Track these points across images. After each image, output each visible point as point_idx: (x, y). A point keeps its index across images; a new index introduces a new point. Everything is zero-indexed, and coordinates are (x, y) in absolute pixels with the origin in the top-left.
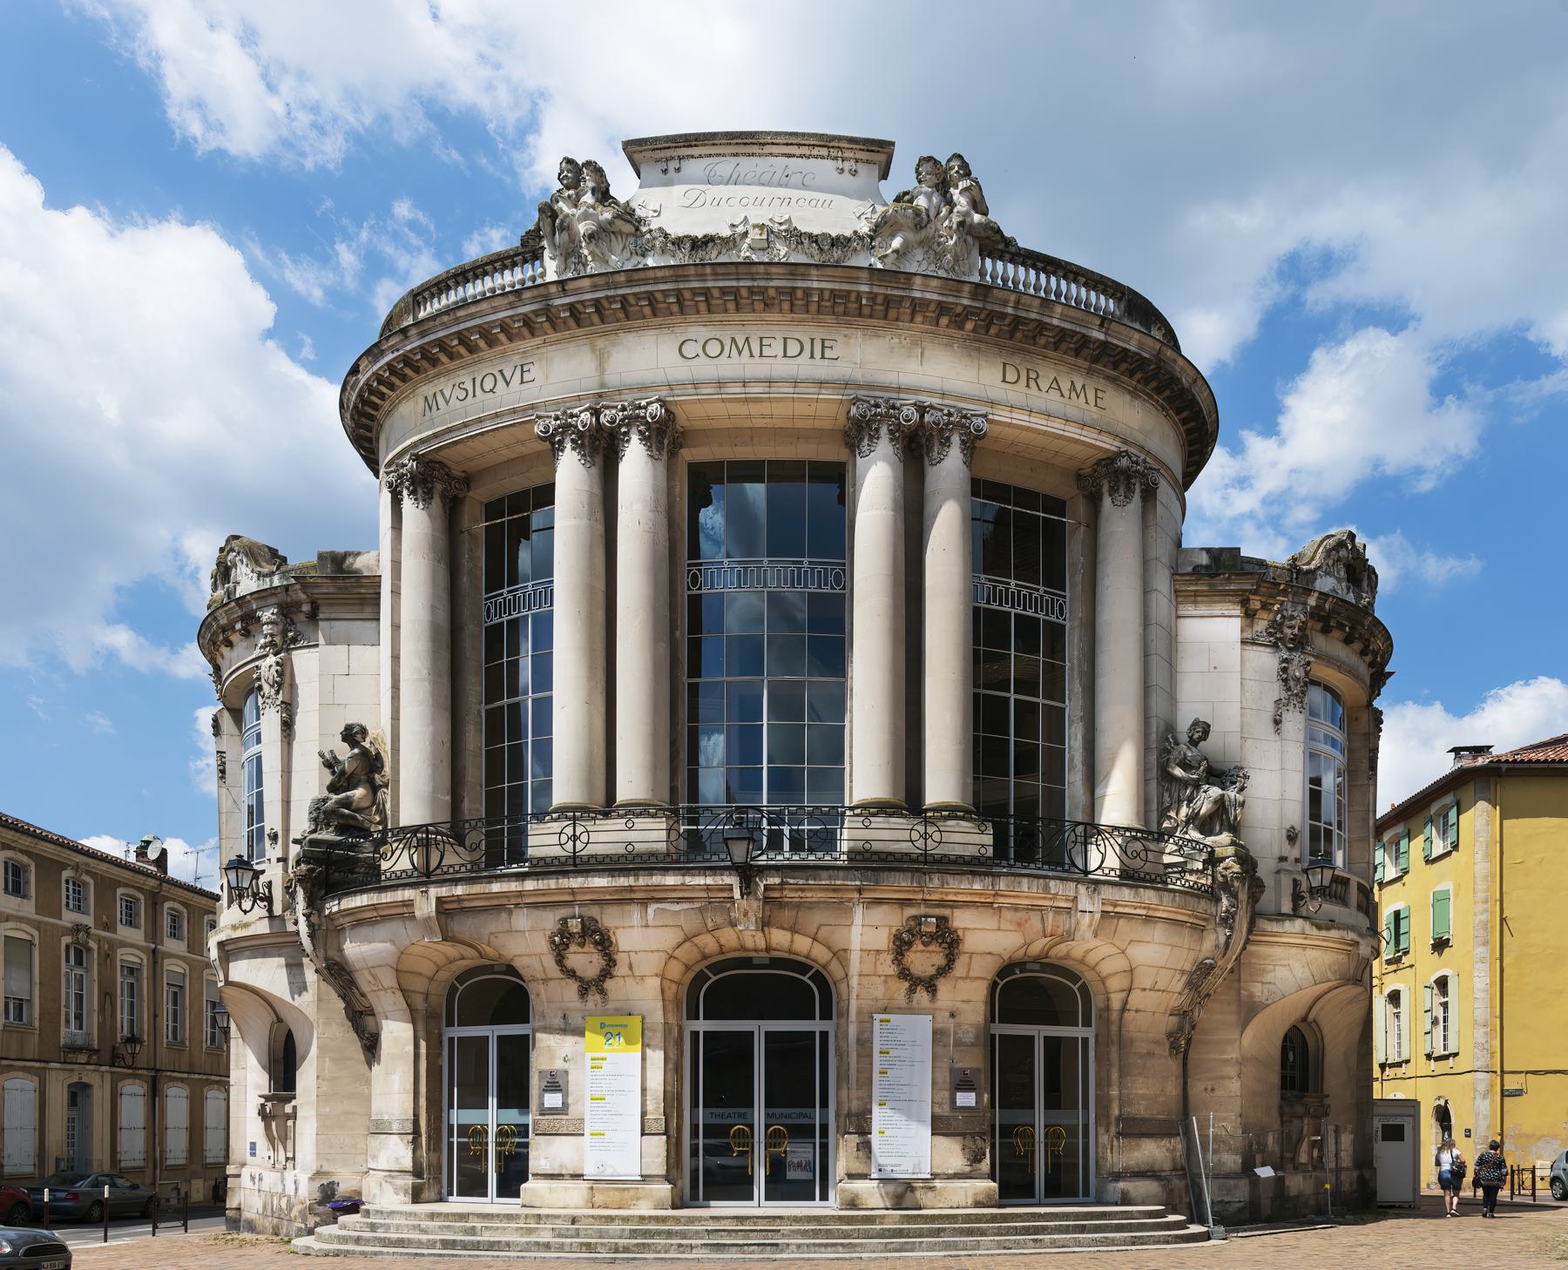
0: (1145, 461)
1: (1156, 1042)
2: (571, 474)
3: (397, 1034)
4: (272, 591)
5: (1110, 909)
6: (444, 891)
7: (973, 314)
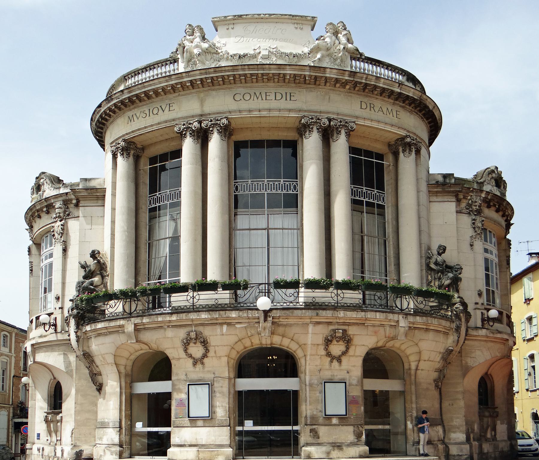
0: (416, 139)
1: (430, 384)
2: (189, 147)
3: (112, 385)
4: (61, 195)
5: (411, 325)
6: (138, 320)
7: (349, 83)
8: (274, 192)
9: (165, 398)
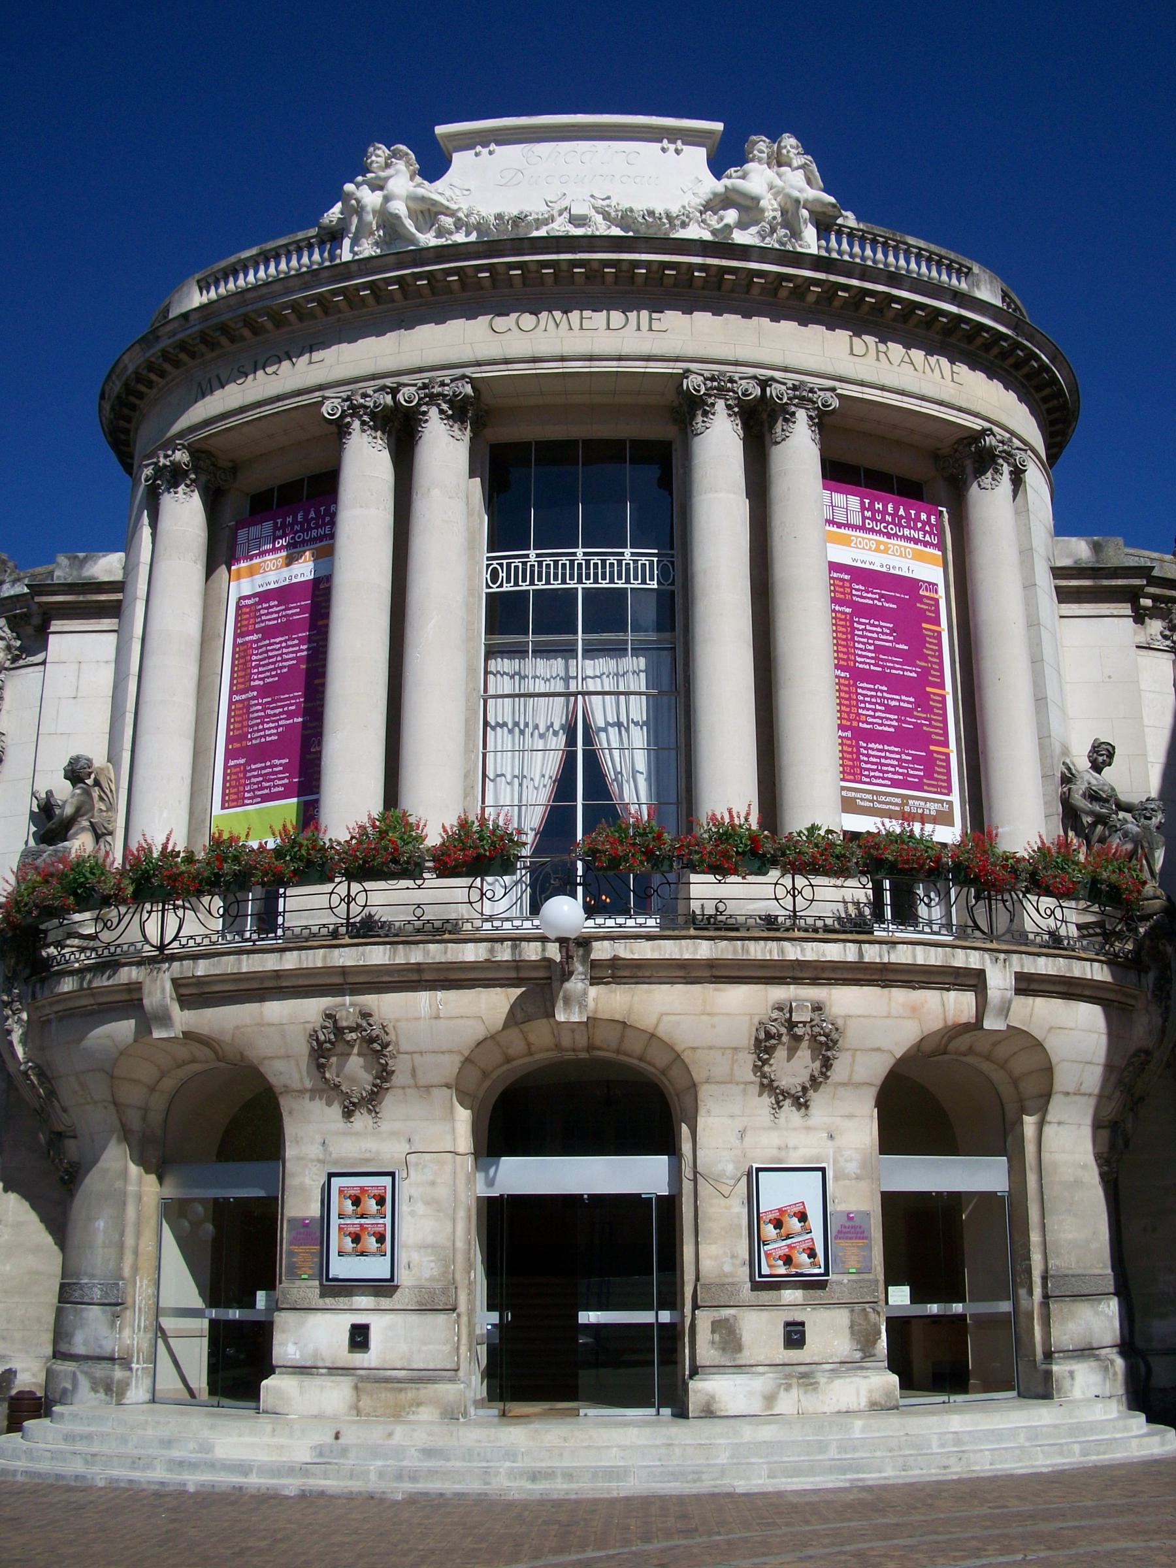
8: (604, 584)
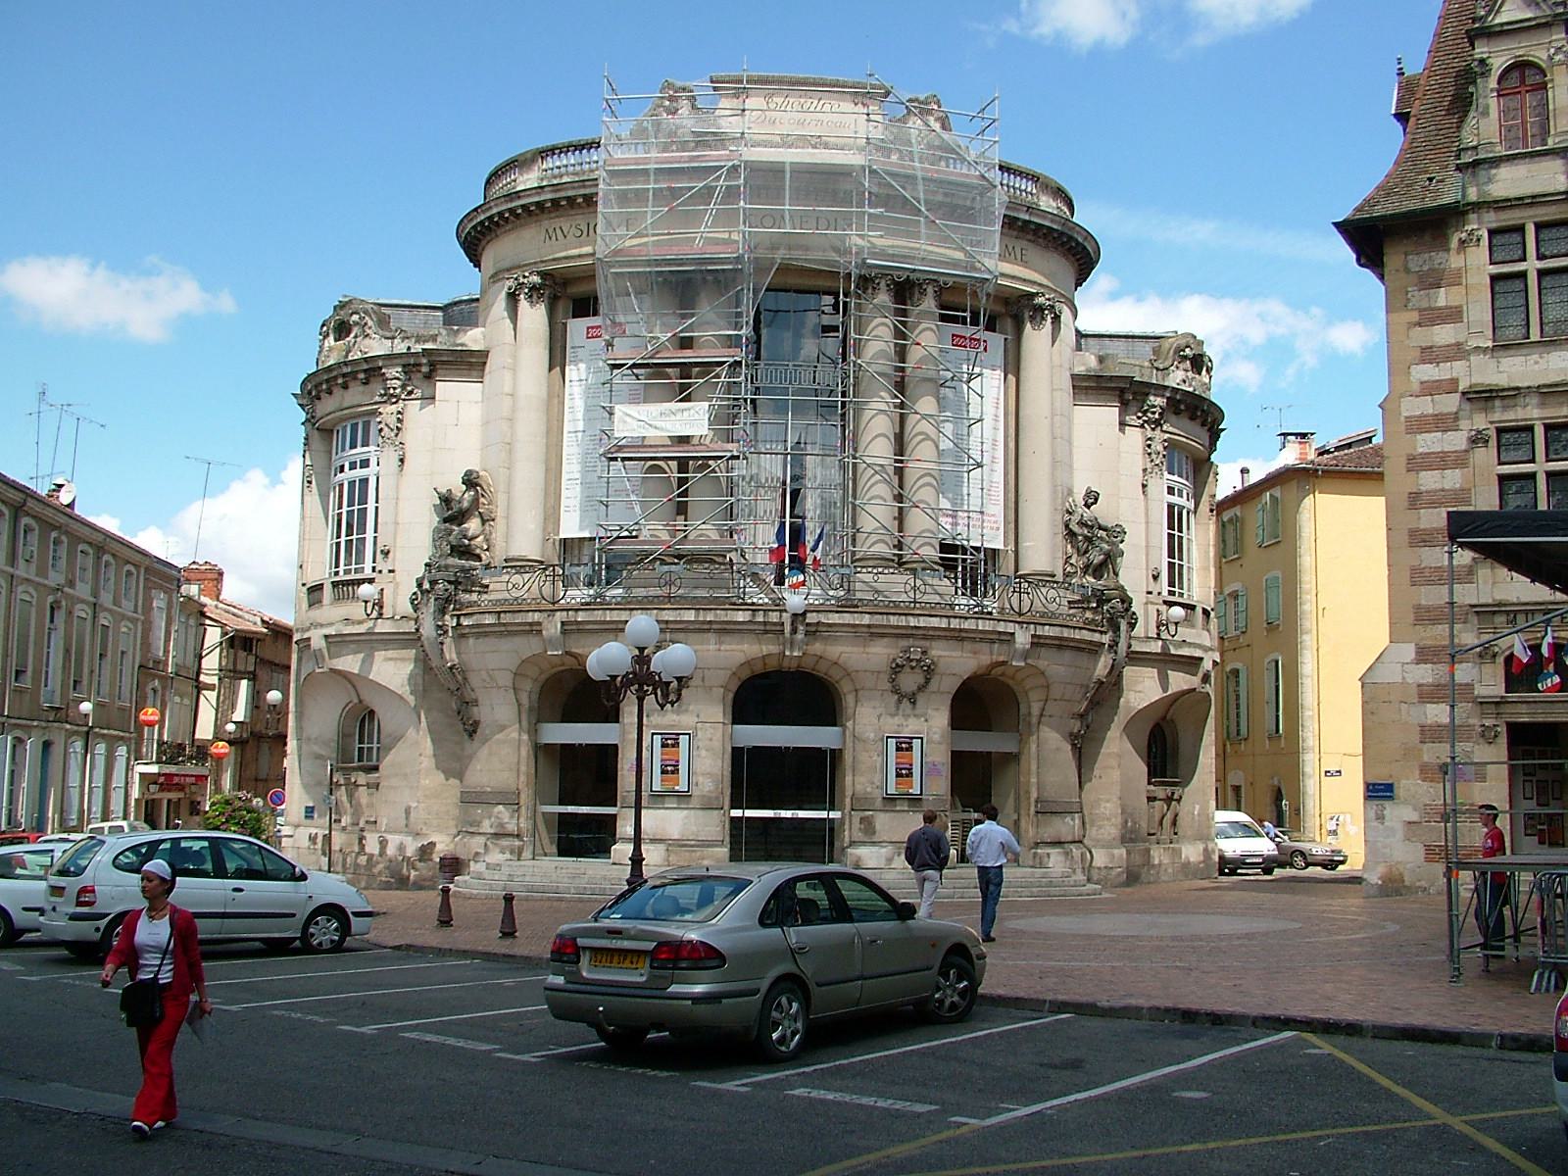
9: (607, 754)
